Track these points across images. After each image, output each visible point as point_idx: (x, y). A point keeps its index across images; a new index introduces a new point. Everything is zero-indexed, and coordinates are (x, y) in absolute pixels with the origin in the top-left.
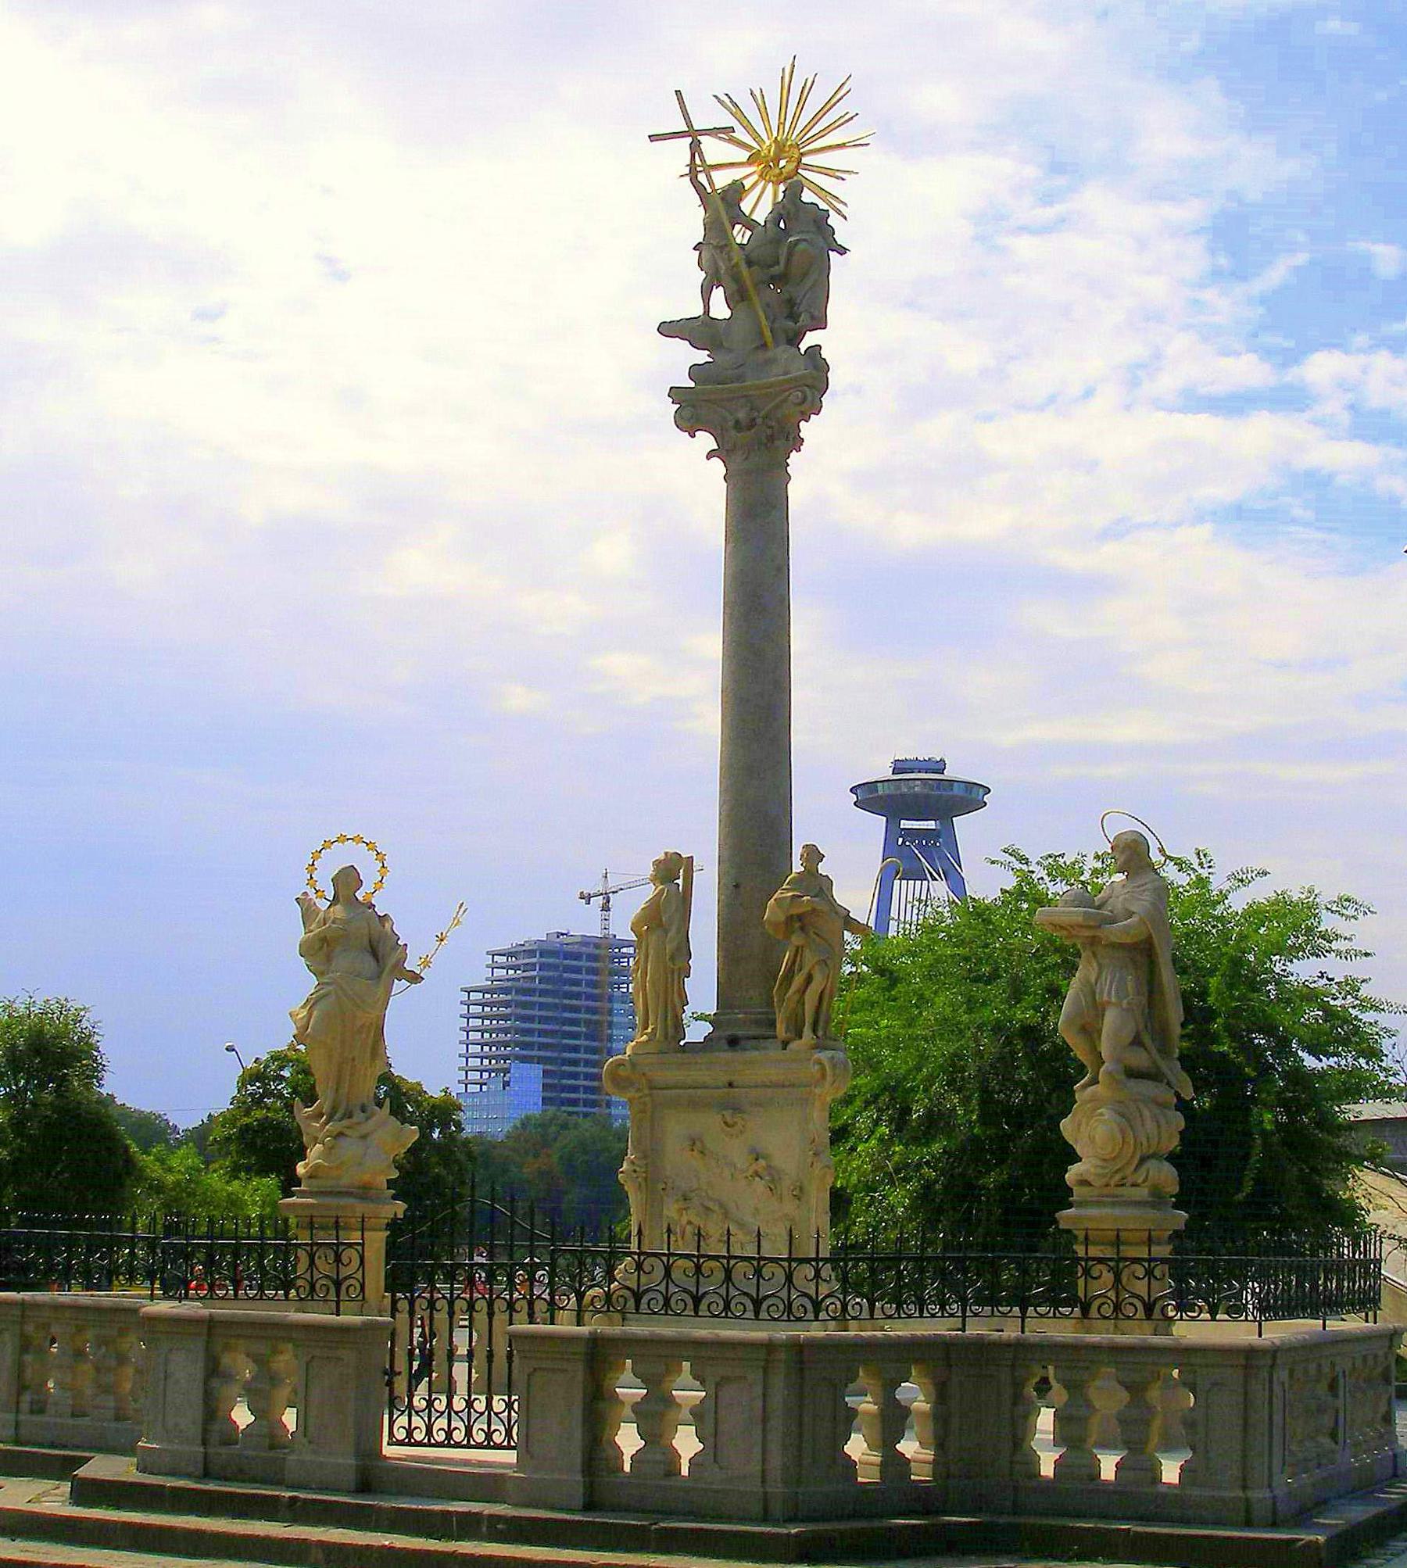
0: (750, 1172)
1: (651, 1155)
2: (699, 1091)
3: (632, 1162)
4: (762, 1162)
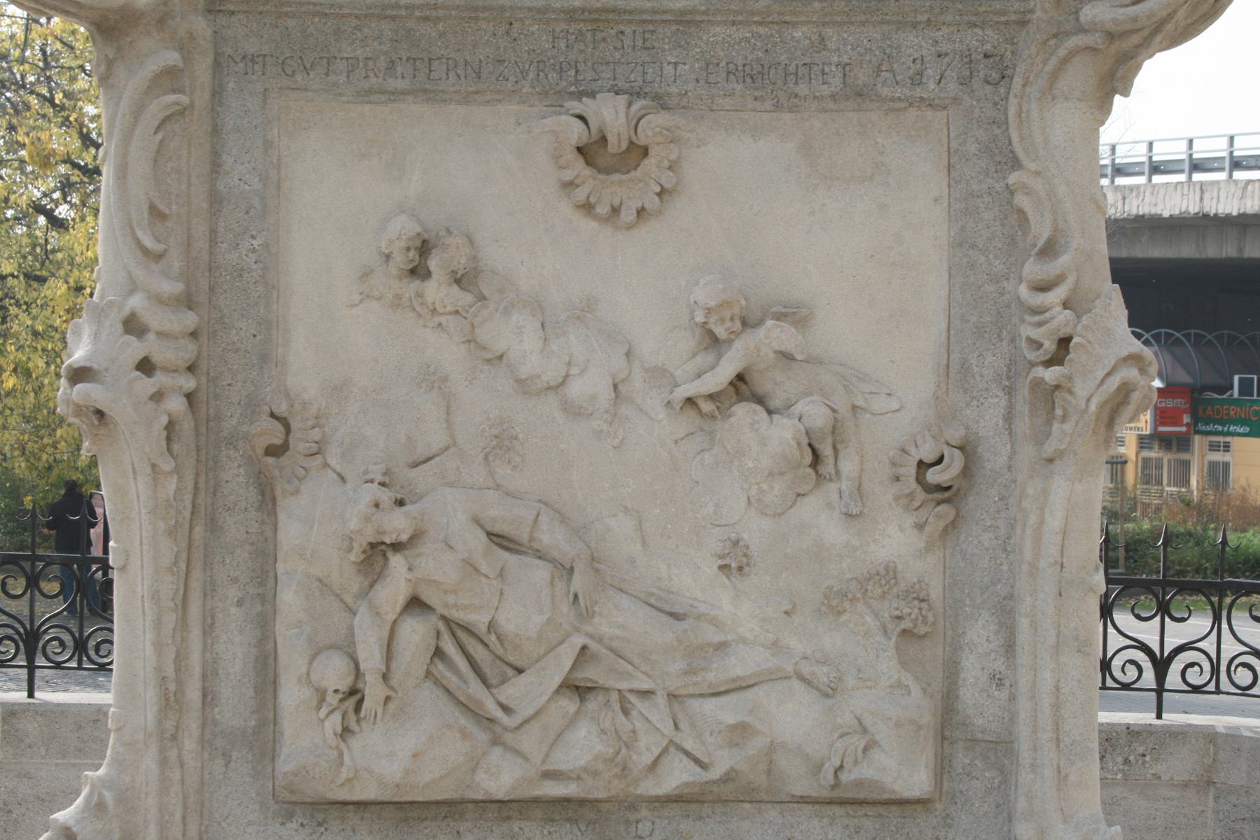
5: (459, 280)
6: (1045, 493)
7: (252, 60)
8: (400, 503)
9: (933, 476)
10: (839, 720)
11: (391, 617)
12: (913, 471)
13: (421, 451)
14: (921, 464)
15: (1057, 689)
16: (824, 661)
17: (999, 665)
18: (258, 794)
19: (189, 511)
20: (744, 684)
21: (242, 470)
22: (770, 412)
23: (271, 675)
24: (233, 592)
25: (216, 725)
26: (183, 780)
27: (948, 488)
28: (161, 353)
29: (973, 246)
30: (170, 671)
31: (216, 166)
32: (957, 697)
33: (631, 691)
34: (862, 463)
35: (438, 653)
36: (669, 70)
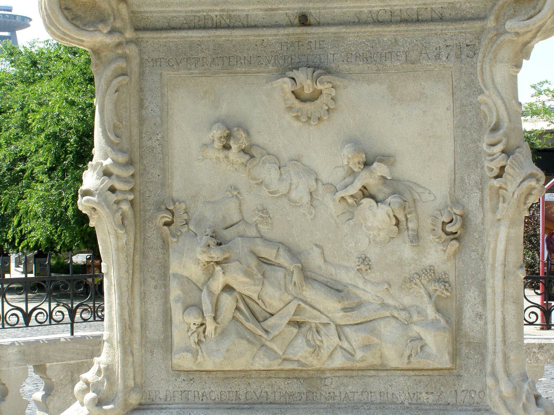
0: (355, 189)
1: (140, 158)
2: (238, 34)
3: (107, 173)
4: (379, 169)
5: (244, 151)
6: (497, 234)
7: (156, 61)
8: (220, 244)
9: (449, 229)
10: (410, 334)
11: (217, 293)
12: (441, 226)
13: (229, 223)
14: (443, 223)
15: (504, 319)
16: (404, 309)
17: (480, 310)
18: (165, 367)
19: (133, 249)
20: (369, 320)
21: (155, 232)
22: (377, 202)
23: (169, 318)
24: (153, 283)
25: (147, 338)
26: (133, 361)
27: (456, 233)
28: (118, 186)
29: (464, 127)
30: (127, 317)
31: (141, 106)
32: (462, 323)
33: (320, 323)
34: (418, 223)
35: (237, 308)
36: (330, 57)
